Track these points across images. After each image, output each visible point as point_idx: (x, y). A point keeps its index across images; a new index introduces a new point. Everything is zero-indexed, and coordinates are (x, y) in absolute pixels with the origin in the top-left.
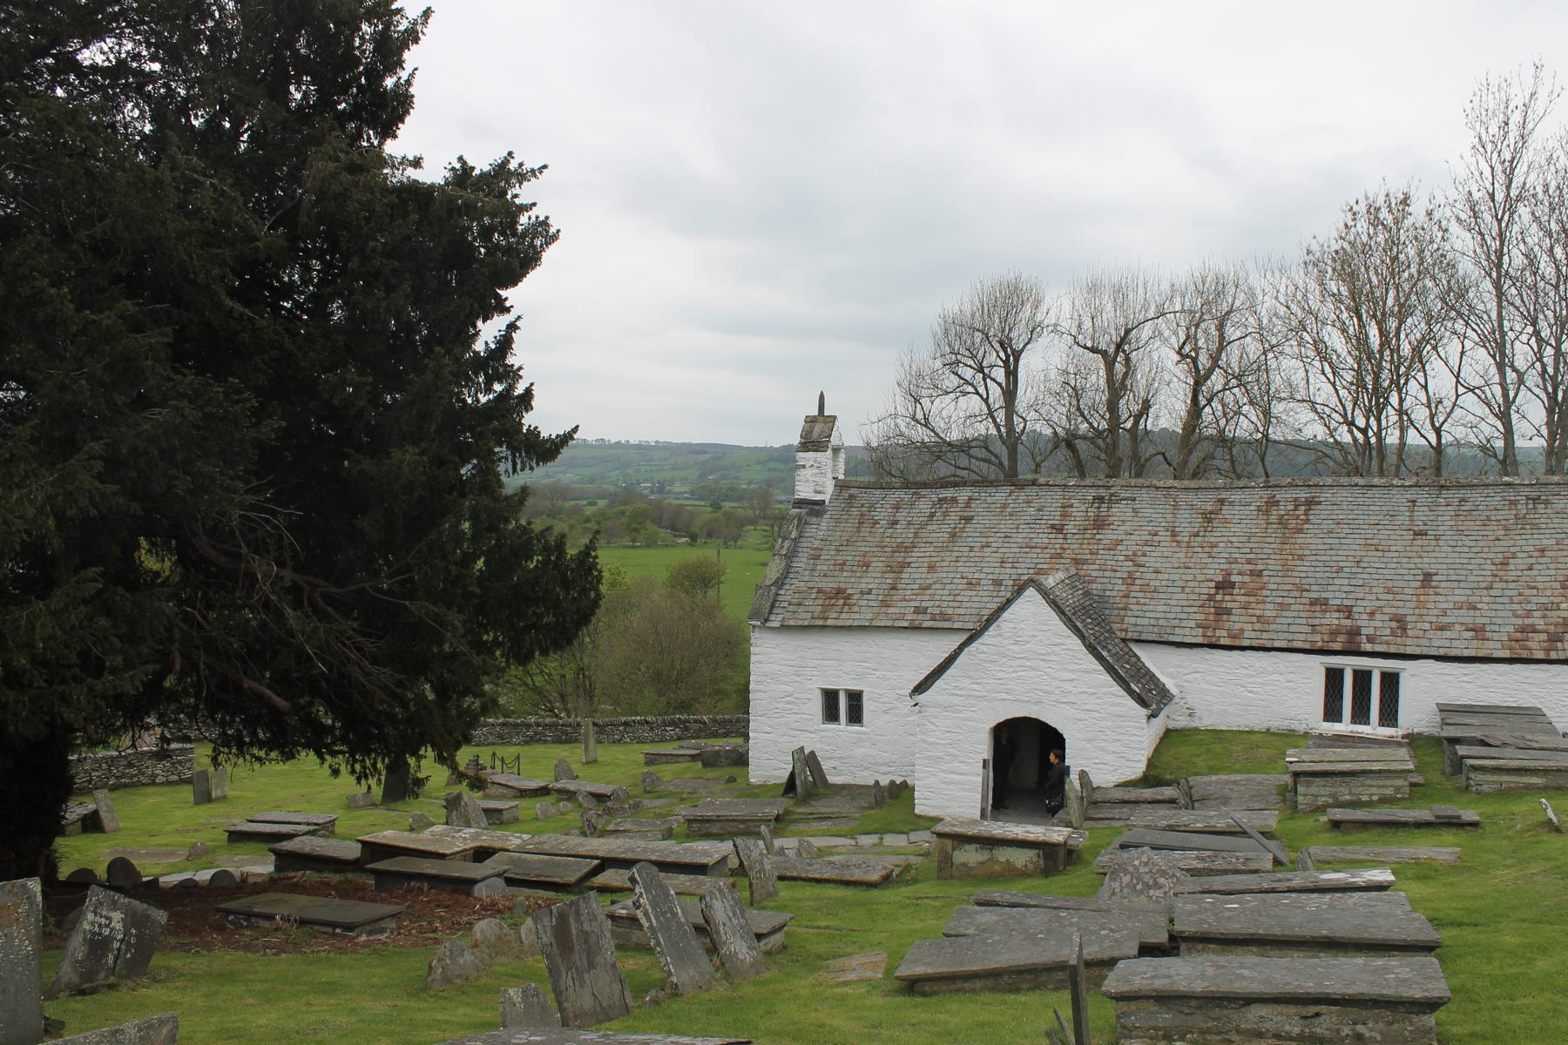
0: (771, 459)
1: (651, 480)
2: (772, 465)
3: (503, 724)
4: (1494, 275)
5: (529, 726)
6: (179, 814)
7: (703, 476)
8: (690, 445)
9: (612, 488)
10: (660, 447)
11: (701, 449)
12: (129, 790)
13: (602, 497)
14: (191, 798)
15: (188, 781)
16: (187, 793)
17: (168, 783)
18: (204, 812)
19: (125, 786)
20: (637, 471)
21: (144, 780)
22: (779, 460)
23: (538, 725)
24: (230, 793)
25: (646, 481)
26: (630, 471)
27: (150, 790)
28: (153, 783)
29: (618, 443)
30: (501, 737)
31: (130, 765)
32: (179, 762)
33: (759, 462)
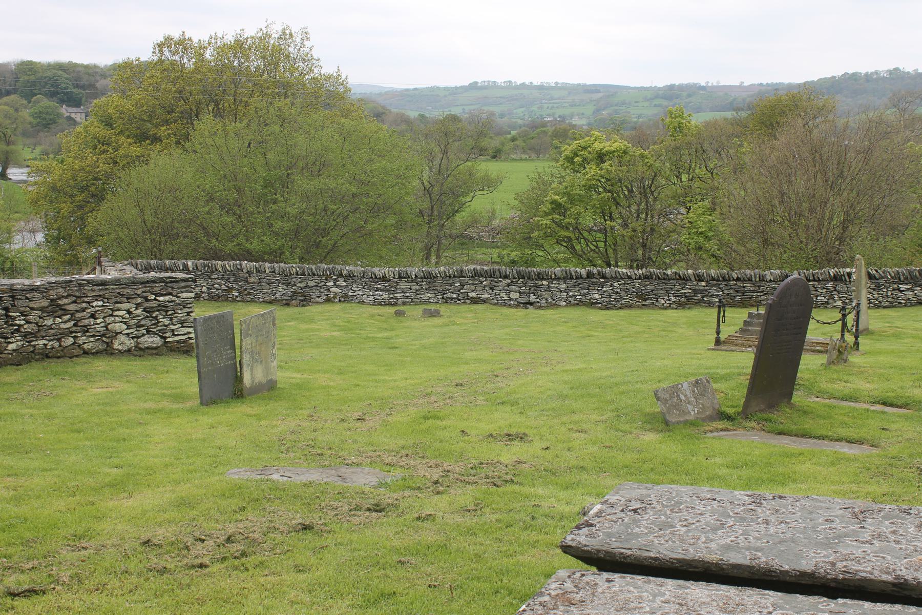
0: (657, 97)
1: (553, 115)
2: (657, 102)
3: (646, 277)
4: (586, 234)
5: (684, 279)
6: (160, 431)
7: (597, 111)
8: (585, 85)
9: (520, 122)
10: (559, 87)
11: (595, 89)
12: (54, 365)
13: (514, 129)
14: (192, 386)
15: (184, 349)
16: (182, 375)
17: (140, 352)
18: (229, 423)
19: (46, 355)
20: (540, 108)
21: (90, 344)
22: (664, 97)
23: (700, 278)
24: (281, 376)
25: (549, 115)
26: (534, 108)
27: (100, 364)
28: (108, 351)
29: (523, 84)
30: (642, 297)
31: (55, 309)
32: (163, 308)
33: (646, 100)
